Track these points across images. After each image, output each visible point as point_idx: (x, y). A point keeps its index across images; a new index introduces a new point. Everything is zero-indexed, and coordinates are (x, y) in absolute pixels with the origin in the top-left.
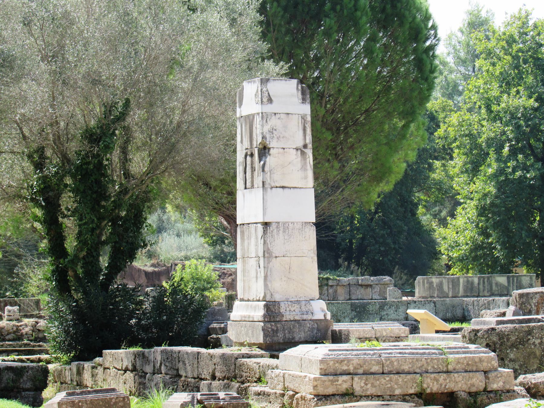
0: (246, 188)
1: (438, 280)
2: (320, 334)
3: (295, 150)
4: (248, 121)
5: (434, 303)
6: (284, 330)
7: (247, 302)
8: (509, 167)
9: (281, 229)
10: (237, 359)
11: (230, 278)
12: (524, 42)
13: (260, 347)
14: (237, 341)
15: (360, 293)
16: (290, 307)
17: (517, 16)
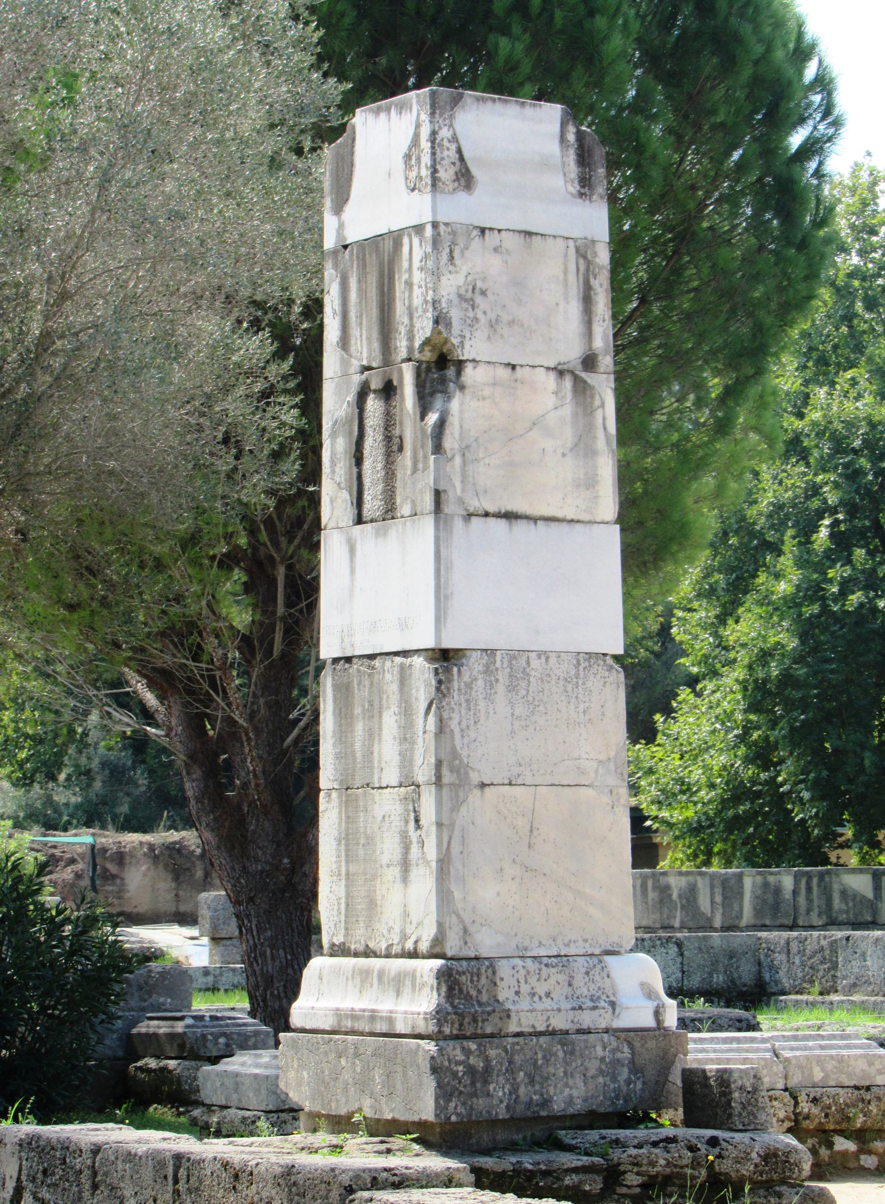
0: (359, 520)
2: (639, 1085)
3: (552, 375)
4: (372, 261)
5: (679, 944)
6: (511, 1071)
7: (362, 961)
8: (831, 581)
10: (350, 1190)
11: (69, 869)
12: (862, 253)
13: (430, 1137)
14: (317, 1108)
16: (533, 980)
17: (848, 182)
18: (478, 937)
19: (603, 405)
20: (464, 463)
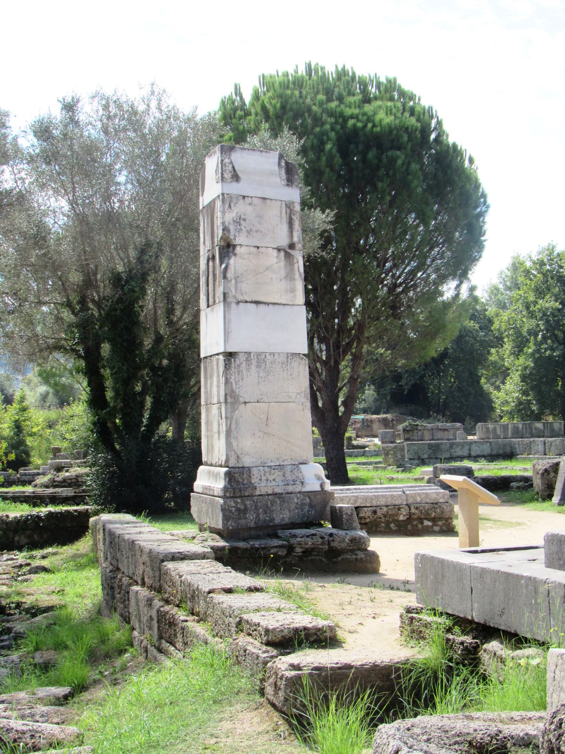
1: (493, 426)
2: (313, 512)
3: (275, 251)
5: (490, 443)
9: (254, 362)
12: (550, 265)
15: (440, 434)
16: (267, 475)
18: (244, 460)
19: (298, 262)
20: (236, 283)
